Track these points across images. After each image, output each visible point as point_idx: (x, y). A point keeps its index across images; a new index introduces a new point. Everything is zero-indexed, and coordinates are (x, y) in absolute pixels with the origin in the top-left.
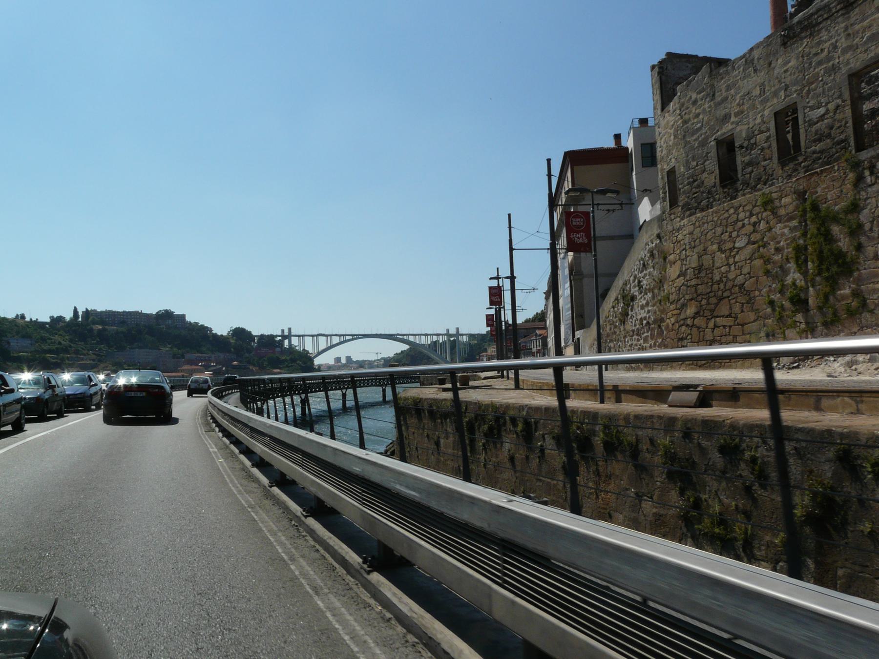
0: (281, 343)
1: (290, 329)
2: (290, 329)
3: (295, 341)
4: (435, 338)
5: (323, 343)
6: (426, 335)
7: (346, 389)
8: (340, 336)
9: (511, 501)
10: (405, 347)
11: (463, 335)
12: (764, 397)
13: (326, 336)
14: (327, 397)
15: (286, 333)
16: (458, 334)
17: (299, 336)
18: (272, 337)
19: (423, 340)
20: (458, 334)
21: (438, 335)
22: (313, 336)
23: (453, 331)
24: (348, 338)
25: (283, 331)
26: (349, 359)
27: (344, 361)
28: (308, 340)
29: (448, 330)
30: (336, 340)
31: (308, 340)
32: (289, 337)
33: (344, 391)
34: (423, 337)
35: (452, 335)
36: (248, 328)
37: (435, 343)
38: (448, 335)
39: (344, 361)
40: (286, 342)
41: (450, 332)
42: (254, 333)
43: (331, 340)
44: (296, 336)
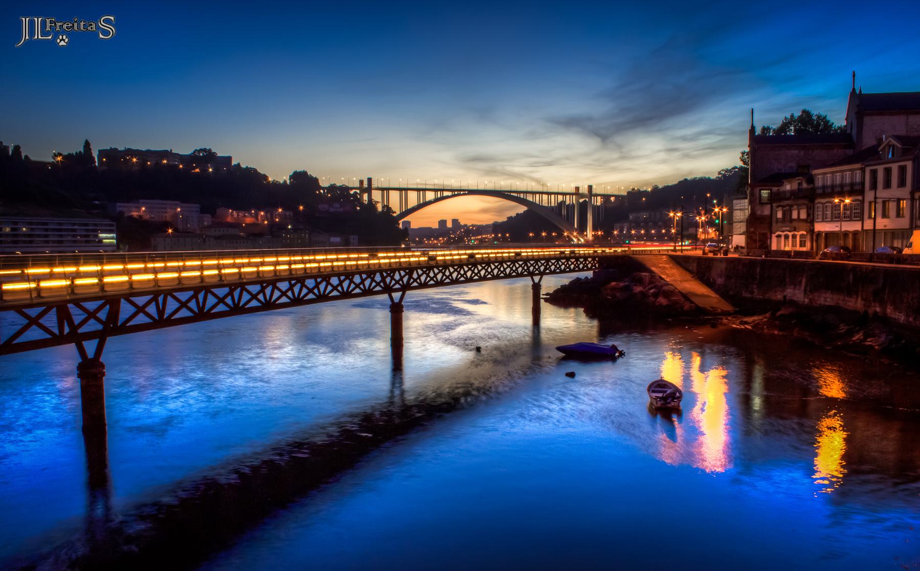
2: (370, 180)
3: (377, 196)
4: (560, 198)
5: (413, 199)
7: (542, 274)
8: (435, 190)
10: (522, 209)
11: (597, 195)
13: (418, 190)
15: (365, 185)
17: (382, 189)
25: (361, 182)
26: (455, 221)
28: (394, 197)
30: (430, 196)
31: (394, 197)
32: (369, 190)
34: (545, 197)
35: (582, 196)
36: (312, 173)
37: (563, 202)
41: (581, 191)
42: (324, 183)
43: (424, 196)
44: (378, 189)
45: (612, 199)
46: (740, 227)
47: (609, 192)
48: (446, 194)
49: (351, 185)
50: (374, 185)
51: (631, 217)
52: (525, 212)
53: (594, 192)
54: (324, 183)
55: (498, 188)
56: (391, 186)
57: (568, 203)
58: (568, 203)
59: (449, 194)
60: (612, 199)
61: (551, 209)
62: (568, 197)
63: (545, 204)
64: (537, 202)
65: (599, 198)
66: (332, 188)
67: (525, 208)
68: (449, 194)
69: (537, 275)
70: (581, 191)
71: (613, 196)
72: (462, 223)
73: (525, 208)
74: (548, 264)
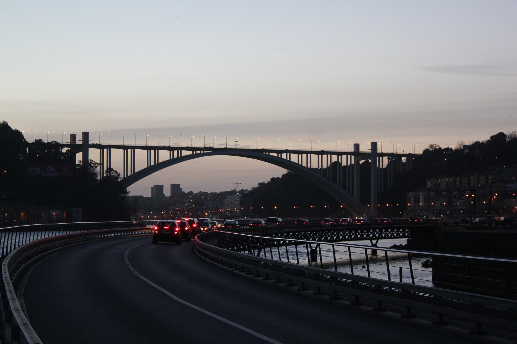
0: (72, 155)
1: (86, 135)
2: (86, 135)
3: (94, 155)
4: (334, 158)
5: (141, 159)
6: (322, 153)
7: (378, 239)
8: (171, 149)
9: (25, 324)
10: (279, 172)
11: (382, 155)
12: (389, 259)
14: (278, 250)
15: (79, 140)
16: (374, 152)
18: (55, 146)
19: (315, 162)
20: (374, 152)
21: (339, 154)
22: (125, 148)
23: (365, 148)
24: (185, 153)
25: (73, 137)
26: (176, 188)
27: (167, 193)
28: (117, 155)
29: (357, 146)
30: (164, 156)
31: (117, 155)
32: (85, 147)
33: (374, 242)
34: (314, 157)
35: (365, 155)
37: (337, 164)
38: (356, 152)
39: (167, 193)
40: (79, 157)
41: (362, 150)
43: (157, 156)
44: (94, 146)
45: (404, 159)
46: (422, 199)
47: (400, 151)
48: (198, 152)
49: (60, 142)
50: (92, 140)
51: (429, 184)
52: (284, 176)
53: (379, 150)
54: (281, 177)
55: (253, 147)
56: (114, 143)
57: (344, 163)
58: (344, 163)
59: (190, 153)
60: (404, 159)
61: (319, 171)
62: (344, 157)
63: (315, 166)
64: (304, 164)
65: (385, 159)
66: (39, 143)
67: (285, 171)
68: (190, 153)
69: (374, 239)
70: (362, 150)
71: (404, 155)
72: (186, 190)
73: (285, 171)
74: (368, 233)
